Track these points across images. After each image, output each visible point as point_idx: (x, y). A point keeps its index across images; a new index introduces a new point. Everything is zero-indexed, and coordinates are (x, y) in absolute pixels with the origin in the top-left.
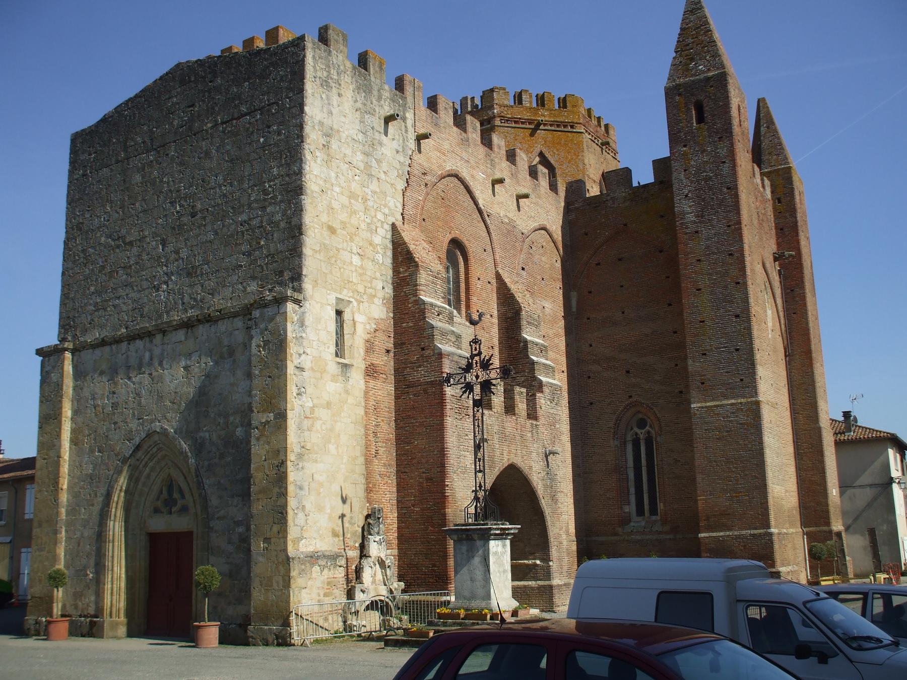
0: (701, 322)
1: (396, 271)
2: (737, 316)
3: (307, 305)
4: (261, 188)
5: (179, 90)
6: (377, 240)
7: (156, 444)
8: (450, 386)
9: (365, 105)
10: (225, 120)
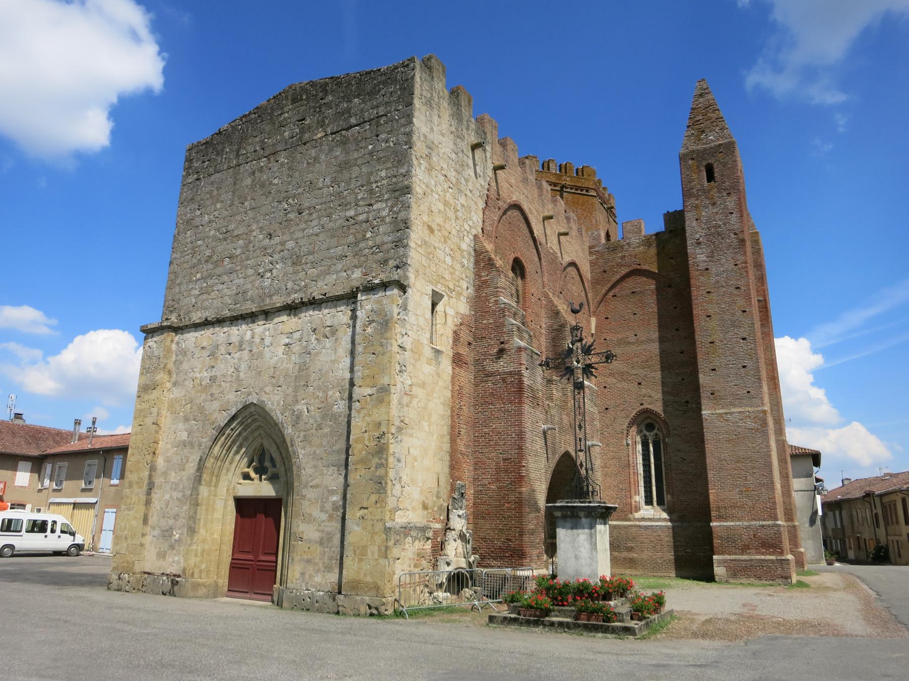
0: (710, 343)
1: (477, 275)
2: (744, 339)
3: (409, 291)
4: (369, 188)
5: (290, 107)
6: (464, 246)
7: (251, 415)
8: (550, 369)
9: (457, 130)
10: (335, 130)
